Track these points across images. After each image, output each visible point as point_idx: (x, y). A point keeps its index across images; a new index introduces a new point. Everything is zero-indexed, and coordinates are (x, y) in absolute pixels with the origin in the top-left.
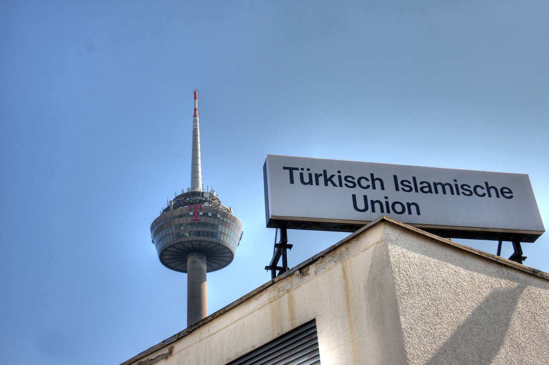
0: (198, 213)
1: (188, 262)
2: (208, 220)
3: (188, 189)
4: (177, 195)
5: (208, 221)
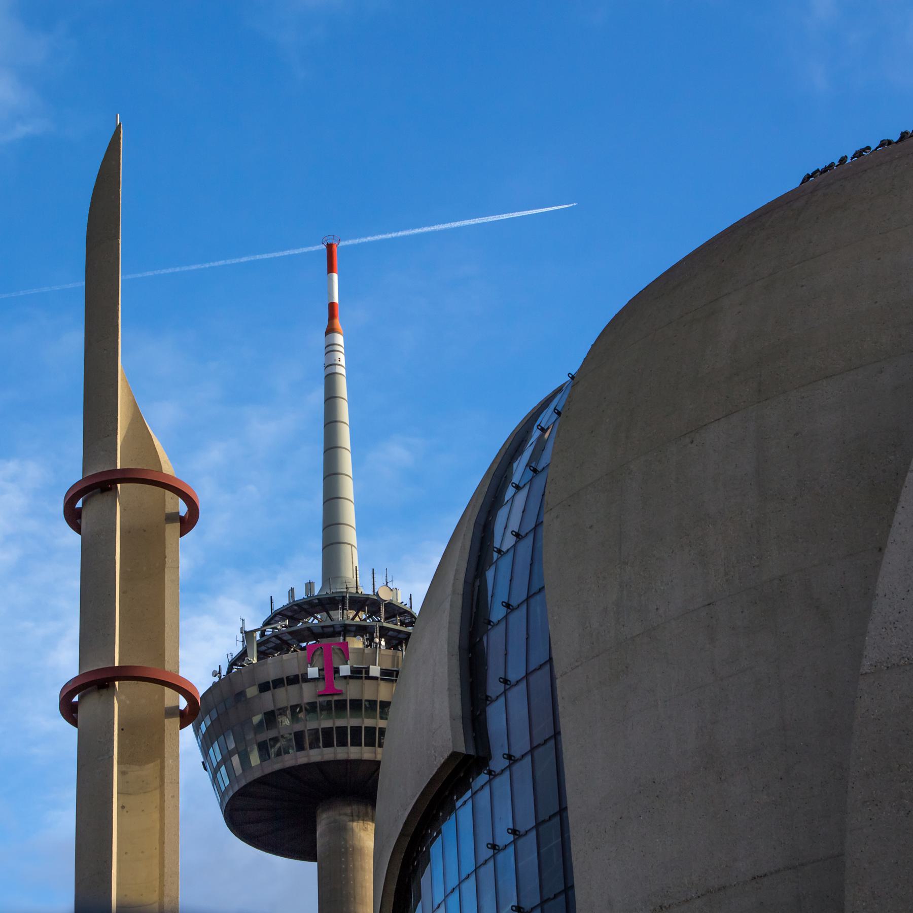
0: (337, 671)
1: (320, 829)
2: (367, 691)
3: (309, 586)
4: (277, 606)
5: (368, 695)
